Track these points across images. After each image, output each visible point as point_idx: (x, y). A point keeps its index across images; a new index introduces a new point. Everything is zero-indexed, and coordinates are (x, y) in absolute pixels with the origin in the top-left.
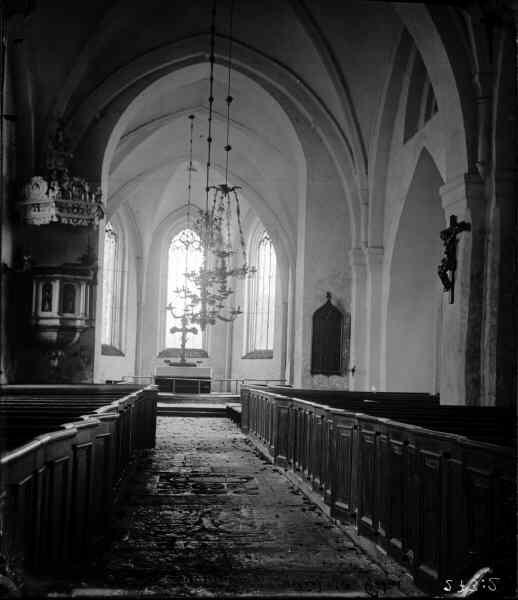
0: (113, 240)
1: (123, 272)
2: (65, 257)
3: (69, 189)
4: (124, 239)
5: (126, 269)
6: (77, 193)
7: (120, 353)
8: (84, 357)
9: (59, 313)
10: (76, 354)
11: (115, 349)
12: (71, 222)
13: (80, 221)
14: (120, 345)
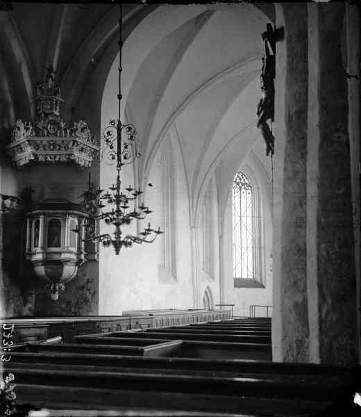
0: (249, 191)
1: (259, 217)
2: (63, 195)
3: (44, 128)
4: (258, 188)
5: (262, 215)
6: (52, 131)
7: (263, 287)
8: (89, 290)
9: (43, 248)
10: (83, 287)
11: (256, 282)
12: (49, 159)
13: (58, 157)
14: (261, 279)
